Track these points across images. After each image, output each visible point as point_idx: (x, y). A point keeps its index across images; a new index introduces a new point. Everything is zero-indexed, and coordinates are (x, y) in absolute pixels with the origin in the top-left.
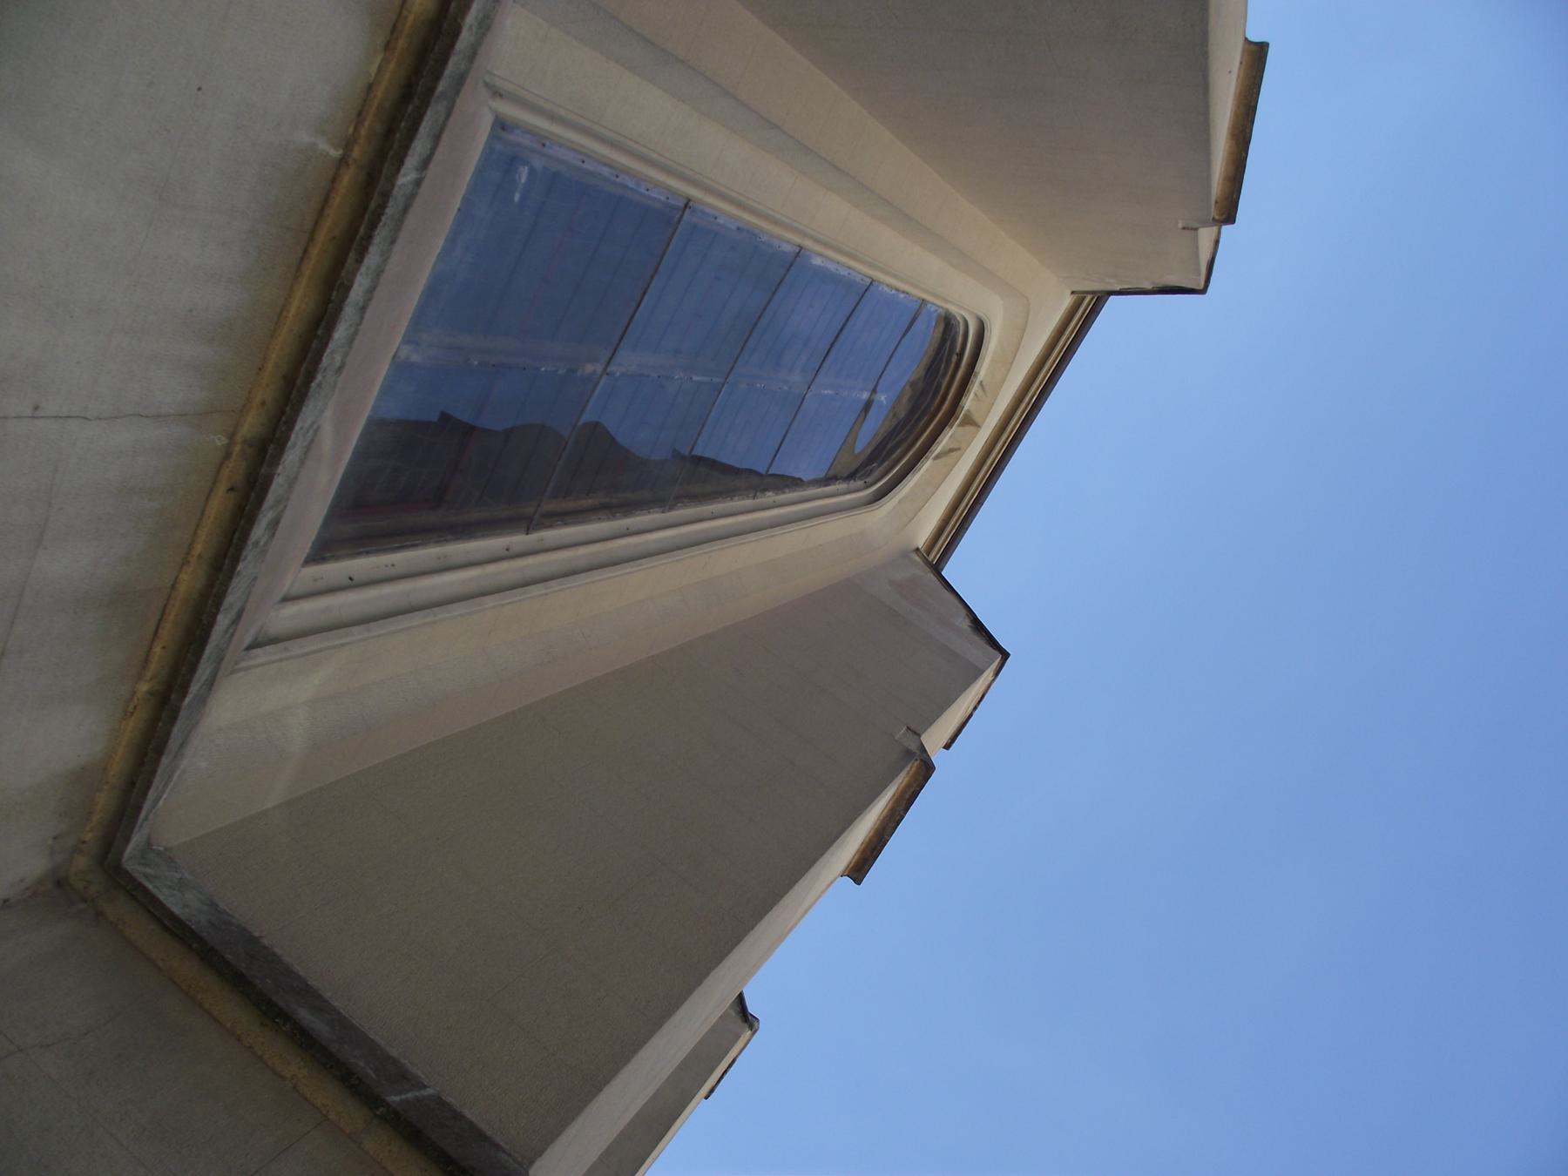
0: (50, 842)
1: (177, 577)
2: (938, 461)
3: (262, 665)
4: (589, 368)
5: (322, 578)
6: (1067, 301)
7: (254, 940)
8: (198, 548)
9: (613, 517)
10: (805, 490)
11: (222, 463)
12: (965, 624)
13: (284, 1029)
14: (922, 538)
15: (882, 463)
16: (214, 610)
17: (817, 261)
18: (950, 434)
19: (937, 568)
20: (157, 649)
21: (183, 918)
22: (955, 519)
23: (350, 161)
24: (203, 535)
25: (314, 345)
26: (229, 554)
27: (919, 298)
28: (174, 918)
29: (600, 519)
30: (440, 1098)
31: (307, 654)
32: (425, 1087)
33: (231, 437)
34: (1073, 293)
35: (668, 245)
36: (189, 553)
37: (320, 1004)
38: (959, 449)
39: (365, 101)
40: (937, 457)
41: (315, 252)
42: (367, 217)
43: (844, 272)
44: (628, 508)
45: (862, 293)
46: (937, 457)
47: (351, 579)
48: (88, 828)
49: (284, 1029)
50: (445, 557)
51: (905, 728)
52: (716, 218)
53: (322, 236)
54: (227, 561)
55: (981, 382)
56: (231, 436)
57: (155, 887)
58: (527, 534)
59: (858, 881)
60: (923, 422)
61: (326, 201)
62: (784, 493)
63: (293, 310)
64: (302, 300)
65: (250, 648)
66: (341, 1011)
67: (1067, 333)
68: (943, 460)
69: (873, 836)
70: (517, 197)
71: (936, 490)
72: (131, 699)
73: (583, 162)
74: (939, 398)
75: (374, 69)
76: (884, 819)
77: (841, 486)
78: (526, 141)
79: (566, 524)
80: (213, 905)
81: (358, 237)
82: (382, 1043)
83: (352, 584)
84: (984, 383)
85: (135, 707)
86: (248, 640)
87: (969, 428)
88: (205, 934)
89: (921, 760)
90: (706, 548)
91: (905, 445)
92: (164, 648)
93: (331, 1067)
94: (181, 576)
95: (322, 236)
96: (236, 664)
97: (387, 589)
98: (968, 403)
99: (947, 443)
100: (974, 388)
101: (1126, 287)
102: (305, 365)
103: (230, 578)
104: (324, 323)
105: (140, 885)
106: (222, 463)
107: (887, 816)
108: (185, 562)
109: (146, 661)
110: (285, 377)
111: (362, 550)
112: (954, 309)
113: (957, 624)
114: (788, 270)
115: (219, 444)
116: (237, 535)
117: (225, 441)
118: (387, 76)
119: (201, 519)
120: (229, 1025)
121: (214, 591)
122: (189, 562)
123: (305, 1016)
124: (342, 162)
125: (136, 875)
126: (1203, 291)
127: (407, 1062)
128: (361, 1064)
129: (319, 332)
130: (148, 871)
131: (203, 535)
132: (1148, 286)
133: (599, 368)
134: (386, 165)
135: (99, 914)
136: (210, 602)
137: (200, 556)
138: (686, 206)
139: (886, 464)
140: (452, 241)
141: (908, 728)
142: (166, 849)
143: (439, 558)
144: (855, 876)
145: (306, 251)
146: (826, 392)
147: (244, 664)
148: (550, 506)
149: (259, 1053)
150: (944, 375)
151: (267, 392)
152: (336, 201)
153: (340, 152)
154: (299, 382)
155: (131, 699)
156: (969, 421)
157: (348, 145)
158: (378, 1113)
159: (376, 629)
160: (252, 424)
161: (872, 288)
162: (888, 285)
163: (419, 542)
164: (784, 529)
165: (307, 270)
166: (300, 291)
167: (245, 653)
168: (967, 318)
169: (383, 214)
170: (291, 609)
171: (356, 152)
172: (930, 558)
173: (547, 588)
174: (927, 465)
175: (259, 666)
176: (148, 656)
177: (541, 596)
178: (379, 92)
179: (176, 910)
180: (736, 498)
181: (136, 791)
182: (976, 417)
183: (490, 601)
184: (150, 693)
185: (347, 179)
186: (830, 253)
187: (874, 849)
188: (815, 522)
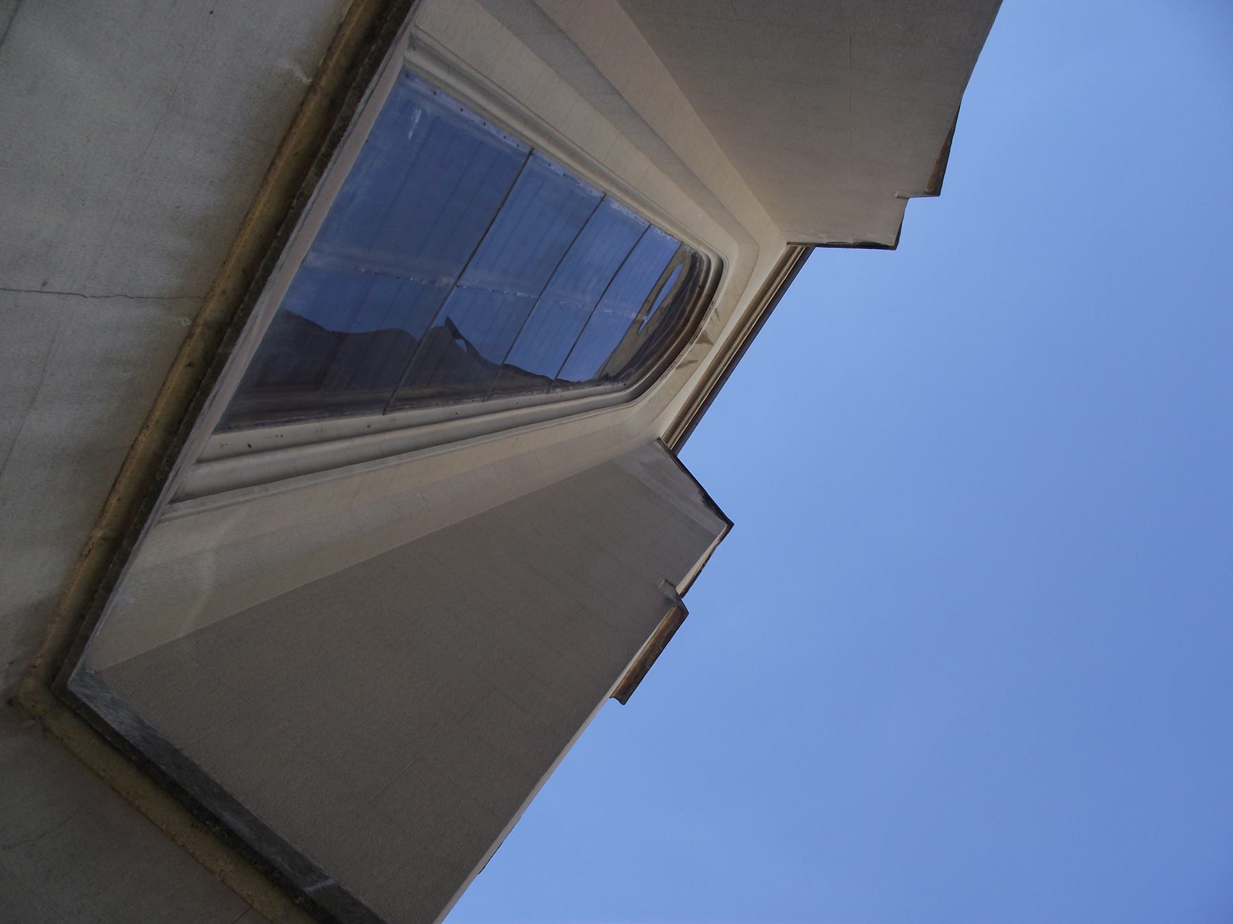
0: (7, 666)
1: (136, 439)
2: (679, 370)
3: (183, 516)
4: (445, 280)
5: (227, 444)
6: (783, 250)
7: (176, 752)
8: (157, 414)
9: (446, 403)
10: (583, 388)
11: (184, 342)
12: (699, 499)
13: (214, 830)
14: (663, 429)
15: (637, 370)
16: (167, 469)
17: (615, 206)
18: (690, 349)
19: (673, 453)
20: (114, 501)
21: (122, 733)
22: (688, 416)
23: (318, 89)
24: (162, 403)
25: (273, 244)
26: (184, 421)
27: (679, 241)
28: (116, 734)
29: (437, 404)
30: (340, 888)
31: (219, 508)
32: (327, 878)
33: (194, 321)
34: (788, 243)
35: (514, 183)
36: (148, 418)
37: (239, 810)
38: (696, 361)
39: (335, 38)
40: (680, 367)
41: (280, 164)
42: (328, 137)
43: (632, 216)
44: (459, 397)
45: (642, 232)
46: (680, 367)
47: (249, 446)
48: (39, 655)
49: (214, 830)
50: (322, 431)
51: (663, 581)
52: (550, 165)
53: (288, 151)
54: (182, 427)
55: (716, 309)
56: (194, 320)
57: (95, 706)
58: (384, 415)
59: (623, 701)
60: (669, 339)
61: (293, 122)
62: (568, 390)
63: (257, 214)
64: (266, 206)
65: (172, 501)
66: (253, 812)
67: (781, 274)
68: (684, 369)
69: (636, 666)
70: (410, 134)
71: (678, 392)
72: (87, 544)
73: (462, 110)
74: (683, 320)
75: (345, 11)
76: (645, 654)
77: (608, 386)
78: (422, 88)
79: (413, 408)
80: (140, 721)
81: (319, 155)
82: (287, 839)
83: (251, 451)
84: (718, 310)
85: (90, 551)
86: (170, 496)
87: (705, 345)
88: (141, 748)
89: (678, 606)
90: (515, 431)
91: (655, 356)
92: (119, 499)
93: (256, 863)
94: (140, 438)
95: (288, 151)
96: (163, 515)
97: (279, 456)
98: (705, 325)
99: (687, 357)
100: (711, 314)
101: (832, 241)
102: (264, 261)
103: (184, 442)
104: (283, 226)
105: (84, 704)
106: (184, 342)
107: (648, 650)
108: (145, 426)
109: (103, 512)
110: (244, 271)
111: (259, 422)
112: (702, 251)
113: (693, 499)
114: (595, 211)
115: (184, 326)
116: (192, 405)
117: (189, 322)
118: (356, 18)
119: (161, 389)
120: (164, 826)
121: (168, 452)
122: (148, 426)
123: (228, 817)
124: (311, 88)
125: (79, 696)
126: (894, 248)
127: (309, 856)
128: (278, 859)
129: (279, 234)
130: (88, 692)
131: (162, 403)
132: (851, 242)
133: (452, 281)
134: (349, 94)
135: (46, 730)
136: (164, 462)
137: (157, 421)
138: (531, 153)
139: (640, 370)
140: (357, 168)
141: (666, 581)
142: (96, 673)
143: (317, 432)
144: (620, 698)
145: (273, 163)
146: (607, 311)
147: (168, 516)
148: (403, 392)
149: (191, 851)
150: (688, 302)
151: (228, 282)
152: (302, 122)
153: (310, 80)
154: (257, 276)
155: (87, 544)
156: (705, 340)
157: (317, 74)
158: (297, 902)
159: (273, 488)
160: (213, 310)
161: (649, 231)
162: (660, 229)
163: (303, 417)
164: (570, 419)
165: (272, 180)
166: (264, 199)
167: (168, 506)
168: (709, 255)
169: (342, 136)
170: (204, 470)
171: (323, 82)
172: (669, 445)
173: (401, 460)
174: (671, 373)
175: (179, 517)
176: (104, 506)
177: (396, 465)
178: (347, 31)
179: (115, 726)
180: (535, 392)
181: (84, 623)
182: (711, 337)
183: (358, 468)
184: (104, 539)
185: (314, 103)
186: (628, 200)
187: (637, 676)
188: (591, 414)
